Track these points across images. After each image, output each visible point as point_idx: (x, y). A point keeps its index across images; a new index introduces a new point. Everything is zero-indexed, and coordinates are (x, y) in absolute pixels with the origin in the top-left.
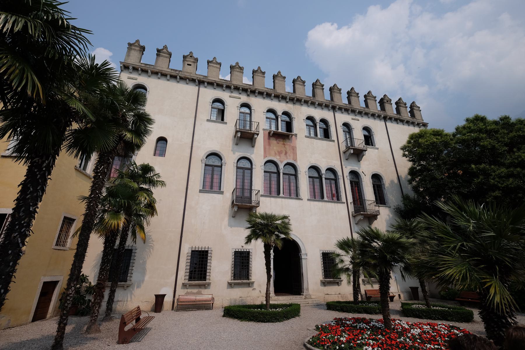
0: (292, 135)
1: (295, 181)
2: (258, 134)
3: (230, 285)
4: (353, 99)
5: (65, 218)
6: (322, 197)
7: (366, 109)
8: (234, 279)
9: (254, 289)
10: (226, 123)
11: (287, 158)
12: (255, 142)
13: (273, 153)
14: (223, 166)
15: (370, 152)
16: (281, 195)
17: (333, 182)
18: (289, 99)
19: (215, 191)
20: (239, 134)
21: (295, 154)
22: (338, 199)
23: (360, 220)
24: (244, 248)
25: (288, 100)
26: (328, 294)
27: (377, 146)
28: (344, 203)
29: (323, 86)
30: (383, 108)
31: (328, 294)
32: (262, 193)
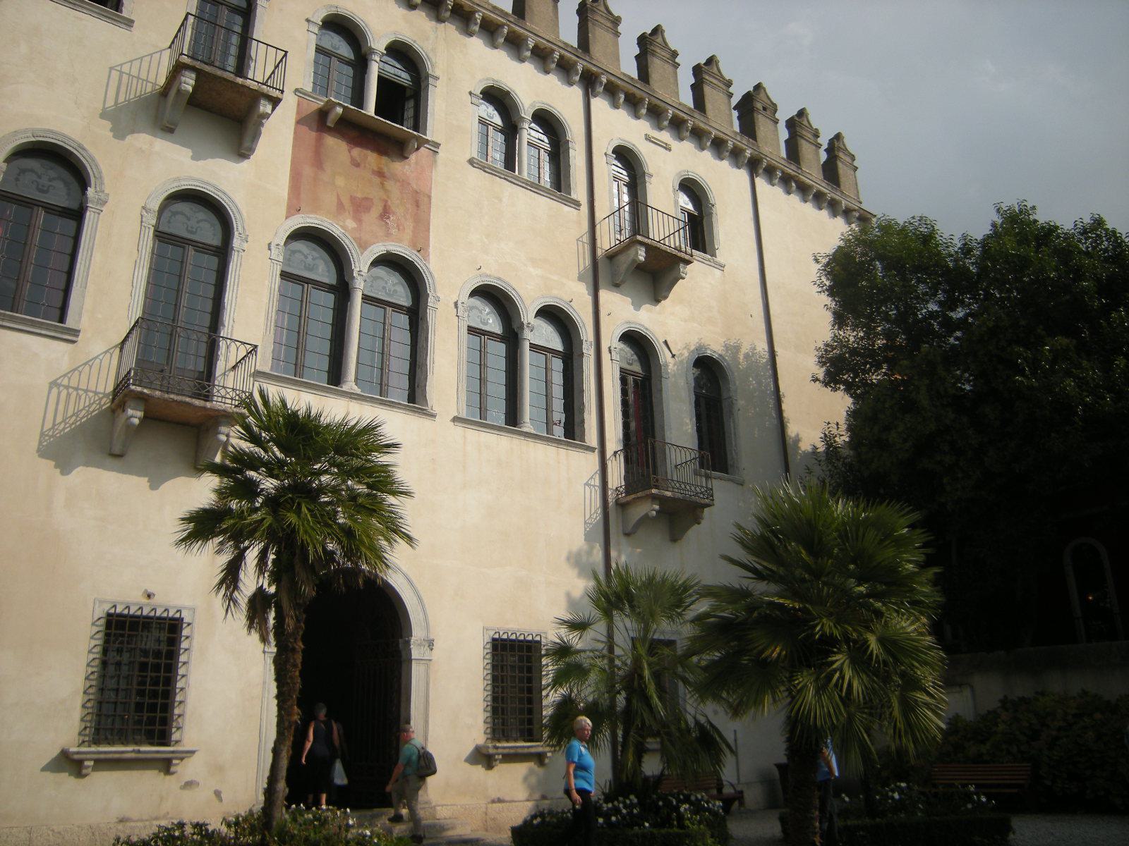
0: (422, 142)
2: (275, 102)
3: (69, 763)
4: (658, 67)
5: (857, 168)
6: (513, 417)
7: (696, 115)
8: (96, 742)
9: (189, 785)
10: (129, 23)
11: (388, 235)
12: (256, 136)
13: (329, 199)
14: (89, 215)
15: (697, 277)
16: (350, 385)
17: (557, 364)
20: (188, 82)
22: (573, 431)
23: (645, 519)
24: (154, 601)
26: (500, 801)
27: (720, 258)
30: (748, 129)
31: (500, 801)
32: (263, 361)
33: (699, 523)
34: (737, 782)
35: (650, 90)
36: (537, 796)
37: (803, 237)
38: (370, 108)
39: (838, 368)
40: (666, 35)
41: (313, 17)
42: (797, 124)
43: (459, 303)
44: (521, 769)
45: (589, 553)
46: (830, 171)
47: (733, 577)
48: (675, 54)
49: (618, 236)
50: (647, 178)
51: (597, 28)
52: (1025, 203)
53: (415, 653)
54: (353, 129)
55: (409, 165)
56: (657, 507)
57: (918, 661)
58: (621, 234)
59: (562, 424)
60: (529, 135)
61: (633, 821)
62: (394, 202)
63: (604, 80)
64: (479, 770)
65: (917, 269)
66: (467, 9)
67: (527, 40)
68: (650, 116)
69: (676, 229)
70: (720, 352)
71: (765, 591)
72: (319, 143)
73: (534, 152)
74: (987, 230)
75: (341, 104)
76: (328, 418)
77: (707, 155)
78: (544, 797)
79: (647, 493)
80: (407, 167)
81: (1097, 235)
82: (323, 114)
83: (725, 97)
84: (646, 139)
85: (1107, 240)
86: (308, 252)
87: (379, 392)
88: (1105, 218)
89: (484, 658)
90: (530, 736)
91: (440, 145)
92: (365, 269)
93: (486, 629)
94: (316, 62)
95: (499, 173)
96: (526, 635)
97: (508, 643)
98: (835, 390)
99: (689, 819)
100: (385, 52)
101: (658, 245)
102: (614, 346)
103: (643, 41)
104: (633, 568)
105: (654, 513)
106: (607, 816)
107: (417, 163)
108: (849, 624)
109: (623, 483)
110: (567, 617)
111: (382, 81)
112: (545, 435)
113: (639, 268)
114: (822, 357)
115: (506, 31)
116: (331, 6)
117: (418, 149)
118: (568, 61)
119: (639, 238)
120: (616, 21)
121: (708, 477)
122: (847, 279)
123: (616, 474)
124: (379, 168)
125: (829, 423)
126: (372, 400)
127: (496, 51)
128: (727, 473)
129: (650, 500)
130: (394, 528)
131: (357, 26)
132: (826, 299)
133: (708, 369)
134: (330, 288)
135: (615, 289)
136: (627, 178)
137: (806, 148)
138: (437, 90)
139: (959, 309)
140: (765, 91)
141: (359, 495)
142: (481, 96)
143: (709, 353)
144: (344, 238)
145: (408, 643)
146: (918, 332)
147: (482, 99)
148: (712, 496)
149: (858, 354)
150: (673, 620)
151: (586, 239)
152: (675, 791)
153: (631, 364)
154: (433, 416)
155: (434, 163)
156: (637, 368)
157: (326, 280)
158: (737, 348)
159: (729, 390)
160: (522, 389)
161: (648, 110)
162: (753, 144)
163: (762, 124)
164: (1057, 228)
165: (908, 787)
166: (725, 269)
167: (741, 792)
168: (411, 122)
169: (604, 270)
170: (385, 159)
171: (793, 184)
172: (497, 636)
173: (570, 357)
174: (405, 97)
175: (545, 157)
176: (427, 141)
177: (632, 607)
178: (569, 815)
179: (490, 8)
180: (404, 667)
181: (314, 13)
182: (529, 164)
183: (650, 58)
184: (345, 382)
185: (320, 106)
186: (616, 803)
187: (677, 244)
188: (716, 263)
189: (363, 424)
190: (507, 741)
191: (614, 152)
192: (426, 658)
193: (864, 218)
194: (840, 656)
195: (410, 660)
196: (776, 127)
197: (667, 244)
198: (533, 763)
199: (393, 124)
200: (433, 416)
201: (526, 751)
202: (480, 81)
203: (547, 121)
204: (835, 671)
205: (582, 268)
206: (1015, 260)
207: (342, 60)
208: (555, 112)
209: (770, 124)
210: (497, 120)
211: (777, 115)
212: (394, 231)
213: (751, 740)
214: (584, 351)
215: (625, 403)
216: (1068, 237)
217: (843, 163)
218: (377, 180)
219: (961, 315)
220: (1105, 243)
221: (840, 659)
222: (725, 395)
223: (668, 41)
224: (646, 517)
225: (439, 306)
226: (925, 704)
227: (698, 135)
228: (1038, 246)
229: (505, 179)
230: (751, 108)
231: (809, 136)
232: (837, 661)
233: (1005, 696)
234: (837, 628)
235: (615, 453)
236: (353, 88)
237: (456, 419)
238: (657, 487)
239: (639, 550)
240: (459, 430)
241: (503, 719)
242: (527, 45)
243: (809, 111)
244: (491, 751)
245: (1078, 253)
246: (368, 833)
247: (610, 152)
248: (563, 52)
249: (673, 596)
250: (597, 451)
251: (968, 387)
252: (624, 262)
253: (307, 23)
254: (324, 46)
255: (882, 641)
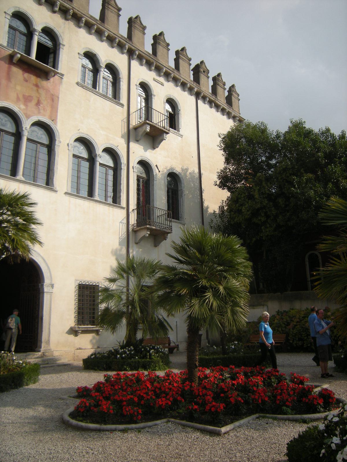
0: (56, 73)
1: (46, 157)
4: (160, 50)
6: (91, 193)
7: (176, 72)
13: (13, 95)
15: (171, 139)
16: (20, 176)
17: (111, 172)
18: (60, 9)
19: (17, 179)
21: (54, 109)
22: (116, 200)
23: (144, 237)
25: (57, 9)
26: (80, 349)
27: (181, 132)
28: (124, 208)
29: (119, 10)
30: (197, 79)
31: (80, 349)
33: (166, 240)
34: (176, 341)
35: (157, 59)
36: (96, 347)
37: (216, 126)
38: (33, 56)
39: (225, 181)
40: (165, 36)
41: (8, 11)
42: (216, 79)
43: (69, 144)
44: (89, 337)
45: (121, 250)
46: (229, 100)
47: (170, 262)
48: (168, 45)
49: (139, 120)
50: (153, 97)
51: (136, 30)
52: (302, 120)
53: (46, 289)
54: (25, 65)
55: (50, 83)
56: (149, 233)
57: (239, 296)
58: (140, 119)
59: (112, 197)
60: (104, 74)
61: (131, 356)
62: (43, 98)
63: (137, 53)
64: (72, 337)
65: (259, 143)
66: (111, 36)
67: (105, 32)
68: (156, 70)
69: (164, 119)
70: (179, 171)
71: (184, 268)
72: (9, 68)
73: (105, 81)
74: (287, 129)
75: (20, 53)
76: (7, 191)
77: (179, 89)
78: (98, 347)
79: (145, 226)
80: (49, 84)
81: (327, 135)
82: (11, 57)
83: (188, 65)
84: (154, 80)
85: (330, 137)
86: (3, 118)
87: (33, 181)
88: (330, 129)
89: (75, 292)
90: (93, 323)
91: (121, 15)
92: (28, 127)
93: (76, 280)
94: (9, 32)
95: (89, 89)
96: (83, 282)
97: (89, 286)
98: (223, 189)
99: (153, 355)
100: (41, 31)
101: (156, 125)
102: (135, 166)
103: (155, 38)
104: (136, 256)
105: (148, 235)
106: (121, 354)
107: (53, 82)
108: (213, 282)
109: (136, 222)
110: (109, 277)
111: (39, 44)
112: (104, 201)
113: (147, 134)
114: (220, 176)
115: (95, 27)
116: (17, 7)
117: (54, 76)
118: (122, 43)
119: (147, 121)
120: (144, 28)
121: (171, 221)
122: (232, 145)
123: (133, 219)
124: (36, 83)
125: (223, 201)
126: (30, 184)
127: (91, 36)
128: (179, 220)
129: (146, 230)
130: (34, 239)
131: (28, 18)
132: (222, 152)
133: (174, 178)
134: (12, 134)
135: (136, 142)
136: (145, 96)
137: (219, 90)
138: (64, 51)
139: (274, 160)
140: (205, 64)
141: (19, 224)
142: (83, 55)
143: (175, 171)
144: (19, 113)
145: (43, 285)
146: (256, 167)
147: (84, 56)
148: (172, 229)
149: (234, 175)
150: (151, 278)
151: (126, 120)
152: (149, 345)
153: (142, 174)
154: (56, 191)
155: (61, 83)
156: (144, 175)
157: (11, 131)
158: (187, 170)
159: (181, 187)
160: (95, 182)
161: (155, 67)
162: (198, 86)
163: (203, 78)
164: (313, 131)
165: (238, 343)
166: (183, 137)
167: (178, 345)
168: (51, 64)
169: (132, 134)
170: (39, 79)
171: (213, 104)
172: (81, 283)
173: (116, 169)
174: (49, 53)
175: (110, 84)
176: (58, 73)
177: (134, 273)
178: (106, 354)
179: (89, 16)
180: (41, 295)
181: (8, 9)
182: (103, 87)
183: (157, 45)
184: (18, 175)
185: (10, 53)
186: (125, 349)
187: (164, 125)
188: (179, 134)
189: (22, 194)
190: (84, 325)
191: (139, 84)
192: (50, 292)
193: (241, 121)
194: (209, 293)
195: (43, 292)
196: (208, 80)
197: (159, 125)
198: (94, 334)
199: (43, 64)
200: (56, 191)
201: (91, 329)
202: (83, 48)
203: (111, 68)
204: (207, 298)
205: (123, 132)
206: (295, 142)
207: (21, 33)
208: (115, 65)
209: (206, 78)
210: (90, 66)
211: (209, 75)
212: (42, 111)
213: (177, 324)
214: (122, 167)
215: (138, 190)
216: (316, 135)
217: (234, 97)
218: (35, 88)
219: (274, 162)
220: (330, 138)
221: (209, 294)
222: (179, 189)
223: (166, 39)
224: (144, 236)
225: (61, 145)
226: (240, 312)
227: (175, 80)
228: (305, 137)
229: (92, 92)
230: (198, 70)
231: (222, 84)
232: (207, 295)
233: (278, 310)
234: (208, 283)
235: (133, 210)
236: (26, 46)
237: (66, 193)
238: (150, 225)
239: (141, 250)
240: (67, 198)
241: (83, 316)
242: (105, 34)
243: (222, 74)
244: (77, 329)
245: (319, 142)
246: (21, 362)
247: (138, 84)
248: (120, 39)
249: (152, 268)
250: (125, 209)
251: (274, 191)
252: (141, 131)
253: (4, 14)
254: (12, 25)
255: (225, 288)
